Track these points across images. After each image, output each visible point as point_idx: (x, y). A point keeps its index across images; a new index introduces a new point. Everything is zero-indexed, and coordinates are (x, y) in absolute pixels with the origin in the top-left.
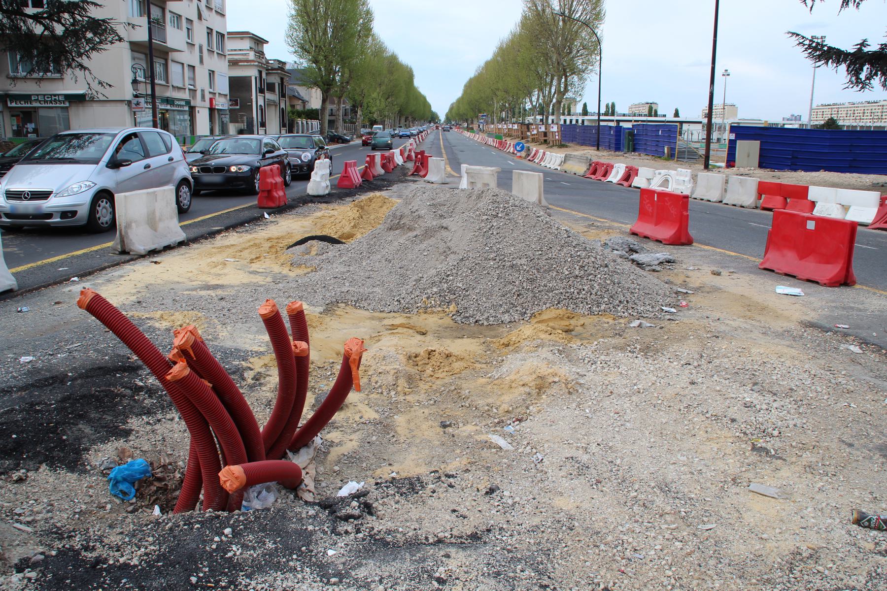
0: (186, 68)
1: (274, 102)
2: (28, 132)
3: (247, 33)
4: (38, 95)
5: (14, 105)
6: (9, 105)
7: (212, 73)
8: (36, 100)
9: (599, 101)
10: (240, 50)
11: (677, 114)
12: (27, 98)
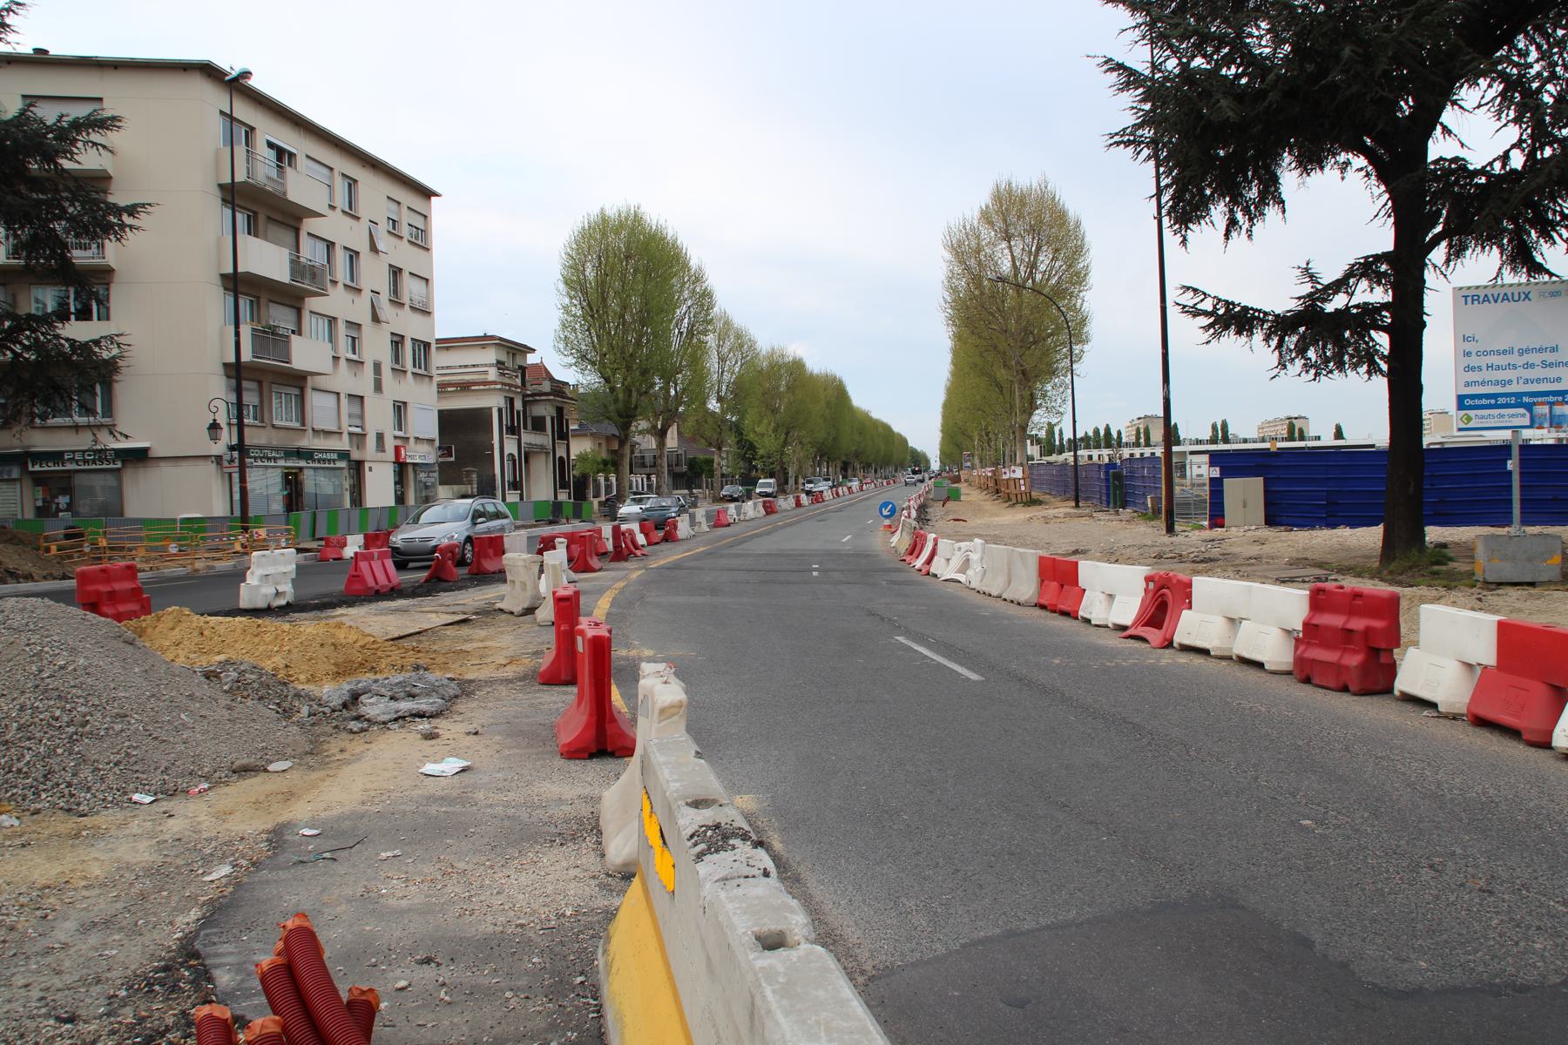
0: (344, 401)
1: (542, 447)
2: (58, 510)
3: (492, 338)
4: (74, 452)
5: (37, 468)
6: (31, 469)
7: (400, 408)
8: (72, 460)
9: (1074, 422)
10: (474, 366)
11: (1339, 434)
12: (57, 456)
